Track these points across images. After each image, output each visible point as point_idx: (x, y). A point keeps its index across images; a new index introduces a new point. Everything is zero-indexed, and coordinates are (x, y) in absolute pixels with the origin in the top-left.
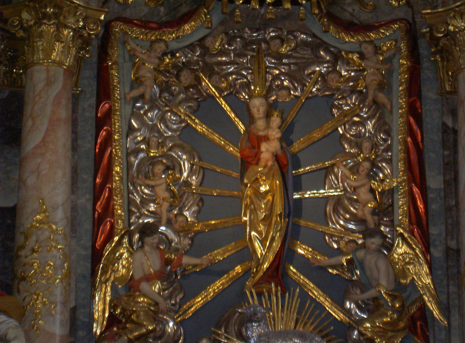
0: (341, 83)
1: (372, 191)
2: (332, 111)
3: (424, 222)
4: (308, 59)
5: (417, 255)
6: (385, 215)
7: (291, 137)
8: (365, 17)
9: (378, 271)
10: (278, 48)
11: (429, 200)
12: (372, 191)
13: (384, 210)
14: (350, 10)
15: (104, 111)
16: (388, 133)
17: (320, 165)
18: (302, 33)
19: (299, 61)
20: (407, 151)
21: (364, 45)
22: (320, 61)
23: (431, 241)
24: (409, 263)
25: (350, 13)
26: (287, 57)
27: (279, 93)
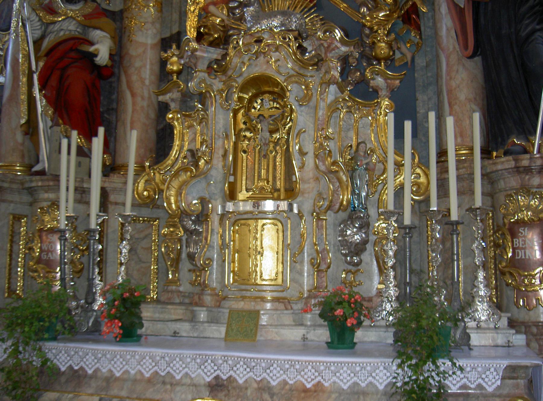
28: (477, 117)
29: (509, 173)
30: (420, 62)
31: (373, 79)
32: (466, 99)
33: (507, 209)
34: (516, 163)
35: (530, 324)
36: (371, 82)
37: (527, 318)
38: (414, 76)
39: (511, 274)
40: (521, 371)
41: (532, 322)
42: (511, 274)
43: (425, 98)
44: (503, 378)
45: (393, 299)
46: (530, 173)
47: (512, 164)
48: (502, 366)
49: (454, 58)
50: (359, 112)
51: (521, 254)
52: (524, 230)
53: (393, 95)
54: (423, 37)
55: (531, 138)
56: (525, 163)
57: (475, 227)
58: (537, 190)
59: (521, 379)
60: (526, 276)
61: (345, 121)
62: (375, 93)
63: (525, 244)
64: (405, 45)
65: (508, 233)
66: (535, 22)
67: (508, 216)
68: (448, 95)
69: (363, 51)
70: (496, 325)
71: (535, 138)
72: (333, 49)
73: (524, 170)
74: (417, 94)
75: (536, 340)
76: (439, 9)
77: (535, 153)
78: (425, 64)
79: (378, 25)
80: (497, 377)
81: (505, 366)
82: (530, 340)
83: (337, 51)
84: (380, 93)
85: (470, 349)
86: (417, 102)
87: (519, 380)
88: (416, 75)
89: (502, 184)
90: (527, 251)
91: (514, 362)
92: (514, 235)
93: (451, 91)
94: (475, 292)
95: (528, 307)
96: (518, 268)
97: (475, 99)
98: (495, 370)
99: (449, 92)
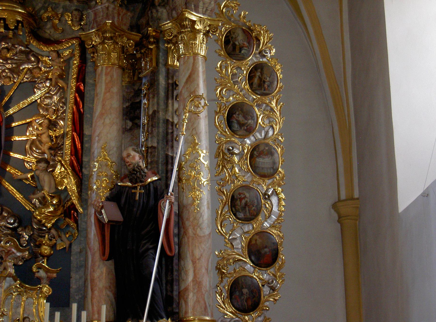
0: (40, 74)
1: (50, 137)
2: (34, 90)
3: (80, 155)
4: (23, 60)
5: (68, 173)
6: (59, 150)
7: (10, 105)
8: (57, 36)
9: (44, 182)
10: (6, 54)
11: (84, 142)
12: (50, 137)
13: (56, 148)
14: (48, 32)
15: (160, 76)
16: (65, 104)
17: (24, 122)
18: (20, 45)
19: (18, 62)
20: (73, 114)
21: (51, 53)
22: (29, 61)
23: (83, 165)
24: (64, 178)
25: (49, 34)
26: (10, 59)
27: (5, 80)
28: (104, 308)
30: (75, 248)
31: (38, 272)
32: (103, 287)
36: (36, 274)
38: (70, 259)
43: (78, 276)
49: (97, 256)
50: (26, 294)
53: (52, 283)
54: (80, 229)
61: (15, 301)
62: (39, 281)
64: (65, 235)
66: (150, 243)
68: (91, 282)
69: (32, 234)
72: (11, 254)
74: (72, 274)
76: (90, 218)
78: (79, 250)
79: (45, 219)
83: (13, 255)
84: (42, 281)
86: (71, 279)
88: (72, 258)
97: (110, 287)
99: (92, 280)
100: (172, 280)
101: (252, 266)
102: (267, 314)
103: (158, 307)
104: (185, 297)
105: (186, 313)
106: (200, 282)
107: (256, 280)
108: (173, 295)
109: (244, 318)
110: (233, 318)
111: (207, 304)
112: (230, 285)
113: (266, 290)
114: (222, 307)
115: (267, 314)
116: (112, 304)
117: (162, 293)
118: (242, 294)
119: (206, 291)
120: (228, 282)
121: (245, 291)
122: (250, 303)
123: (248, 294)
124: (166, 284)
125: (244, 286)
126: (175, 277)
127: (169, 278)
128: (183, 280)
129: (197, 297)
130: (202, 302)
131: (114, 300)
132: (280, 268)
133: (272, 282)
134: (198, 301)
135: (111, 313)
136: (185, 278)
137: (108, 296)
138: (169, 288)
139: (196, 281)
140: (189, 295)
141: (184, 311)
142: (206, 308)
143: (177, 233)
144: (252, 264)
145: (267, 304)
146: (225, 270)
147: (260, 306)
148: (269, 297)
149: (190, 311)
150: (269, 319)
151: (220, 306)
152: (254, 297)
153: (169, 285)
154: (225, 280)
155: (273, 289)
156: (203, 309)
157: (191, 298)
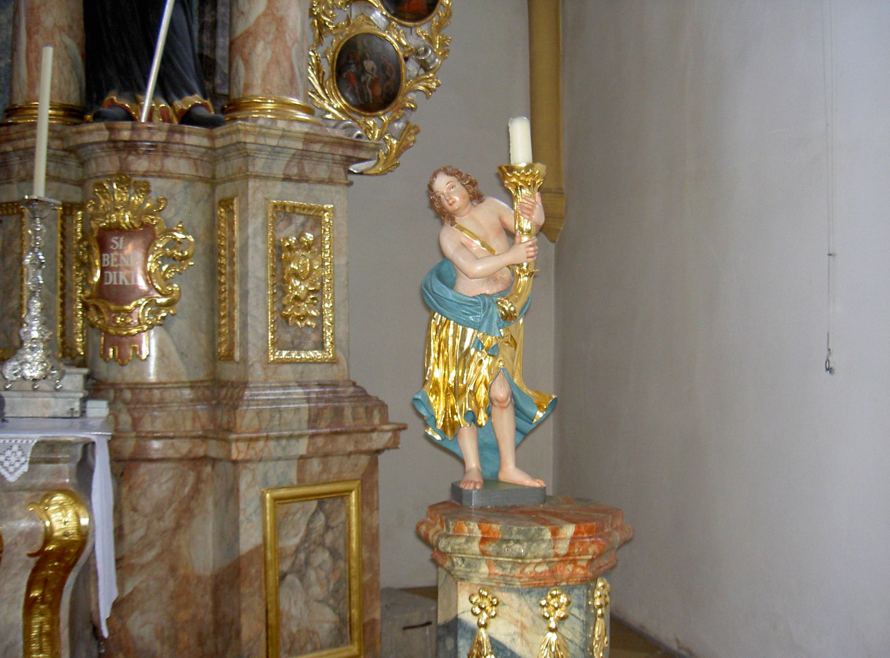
29: (103, 149)
33: (96, 207)
34: (110, 135)
35: (123, 386)
37: (119, 378)
39: (97, 309)
40: (64, 449)
41: (127, 384)
42: (97, 309)
44: (32, 462)
45: (16, 363)
46: (134, 153)
47: (105, 135)
48: (30, 441)
51: (112, 279)
52: (118, 240)
55: (140, 97)
56: (126, 135)
57: (32, 230)
58: (143, 179)
59: (65, 462)
60: (118, 313)
63: (118, 262)
65: (96, 244)
67: (98, 217)
70: (57, 384)
71: (145, 98)
73: (125, 146)
75: (129, 410)
77: (143, 120)
80: (23, 459)
81: (35, 441)
82: (120, 411)
85: (4, 420)
87: (61, 465)
89: (93, 167)
90: (121, 273)
91: (50, 435)
92: (104, 247)
93: (33, 9)
94: (25, 333)
95: (121, 360)
96: (109, 300)
97: (70, 27)
98: (20, 448)
100: (215, 25)
101: (385, 16)
102: (413, 118)
103: (183, 67)
104: (246, 51)
105: (247, 86)
106: (282, 19)
107: (392, 44)
108: (214, 55)
109: (365, 123)
110: (341, 121)
111: (296, 70)
112: (339, 50)
113: (411, 68)
114: (319, 96)
115: (413, 118)
116: (74, 67)
117: (193, 47)
118: (364, 71)
119: (296, 41)
120: (332, 44)
121: (369, 65)
122: (378, 91)
123: (375, 71)
124: (201, 31)
125: (368, 55)
126: (220, 18)
127: (208, 19)
128: (243, 13)
129: (273, 52)
130: (286, 64)
131: (79, 59)
132: (439, 28)
133: (426, 51)
134: (275, 61)
135: (72, 88)
136: (247, 7)
137: (66, 47)
138: (206, 39)
139: (274, 14)
140: (255, 46)
141: (242, 83)
142: (292, 80)
143: (150, 457)
144: (384, 13)
145: (411, 96)
146: (328, 17)
147: (399, 98)
148: (418, 82)
149: (257, 80)
150: (415, 127)
151: (315, 92)
152: (388, 78)
153: (209, 34)
154: (326, 40)
155: (425, 66)
156: (287, 81)
157: (261, 53)
